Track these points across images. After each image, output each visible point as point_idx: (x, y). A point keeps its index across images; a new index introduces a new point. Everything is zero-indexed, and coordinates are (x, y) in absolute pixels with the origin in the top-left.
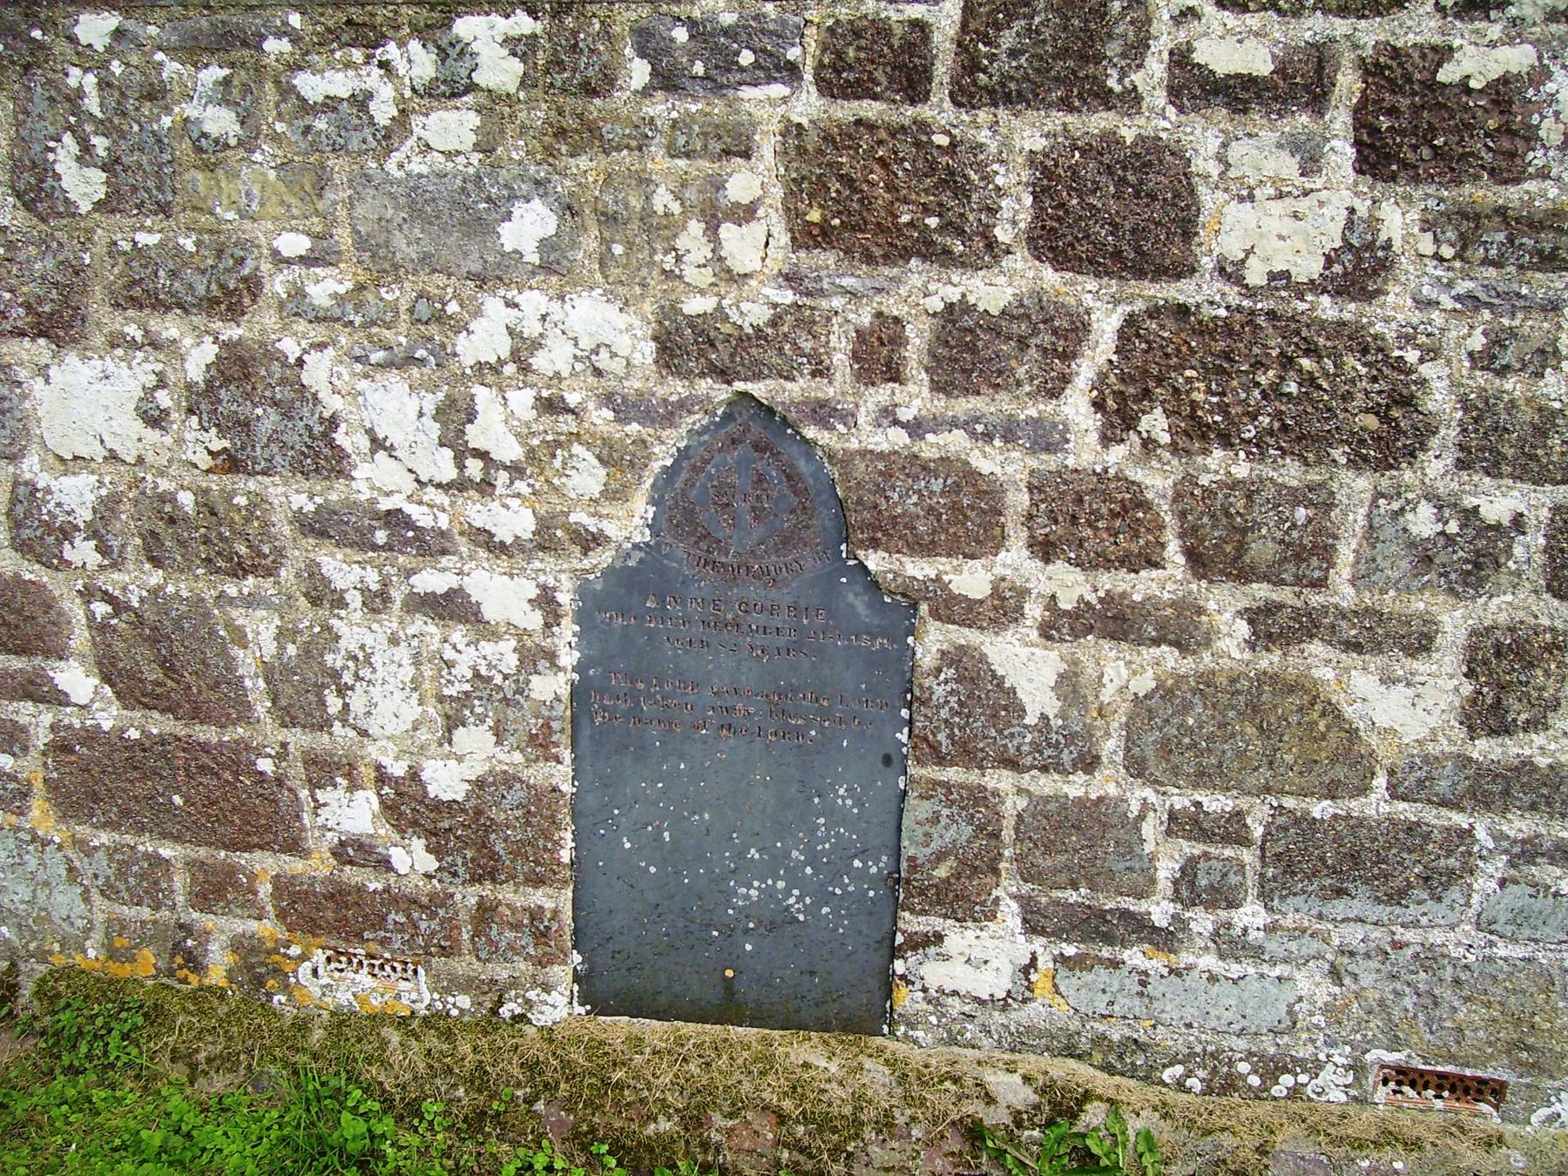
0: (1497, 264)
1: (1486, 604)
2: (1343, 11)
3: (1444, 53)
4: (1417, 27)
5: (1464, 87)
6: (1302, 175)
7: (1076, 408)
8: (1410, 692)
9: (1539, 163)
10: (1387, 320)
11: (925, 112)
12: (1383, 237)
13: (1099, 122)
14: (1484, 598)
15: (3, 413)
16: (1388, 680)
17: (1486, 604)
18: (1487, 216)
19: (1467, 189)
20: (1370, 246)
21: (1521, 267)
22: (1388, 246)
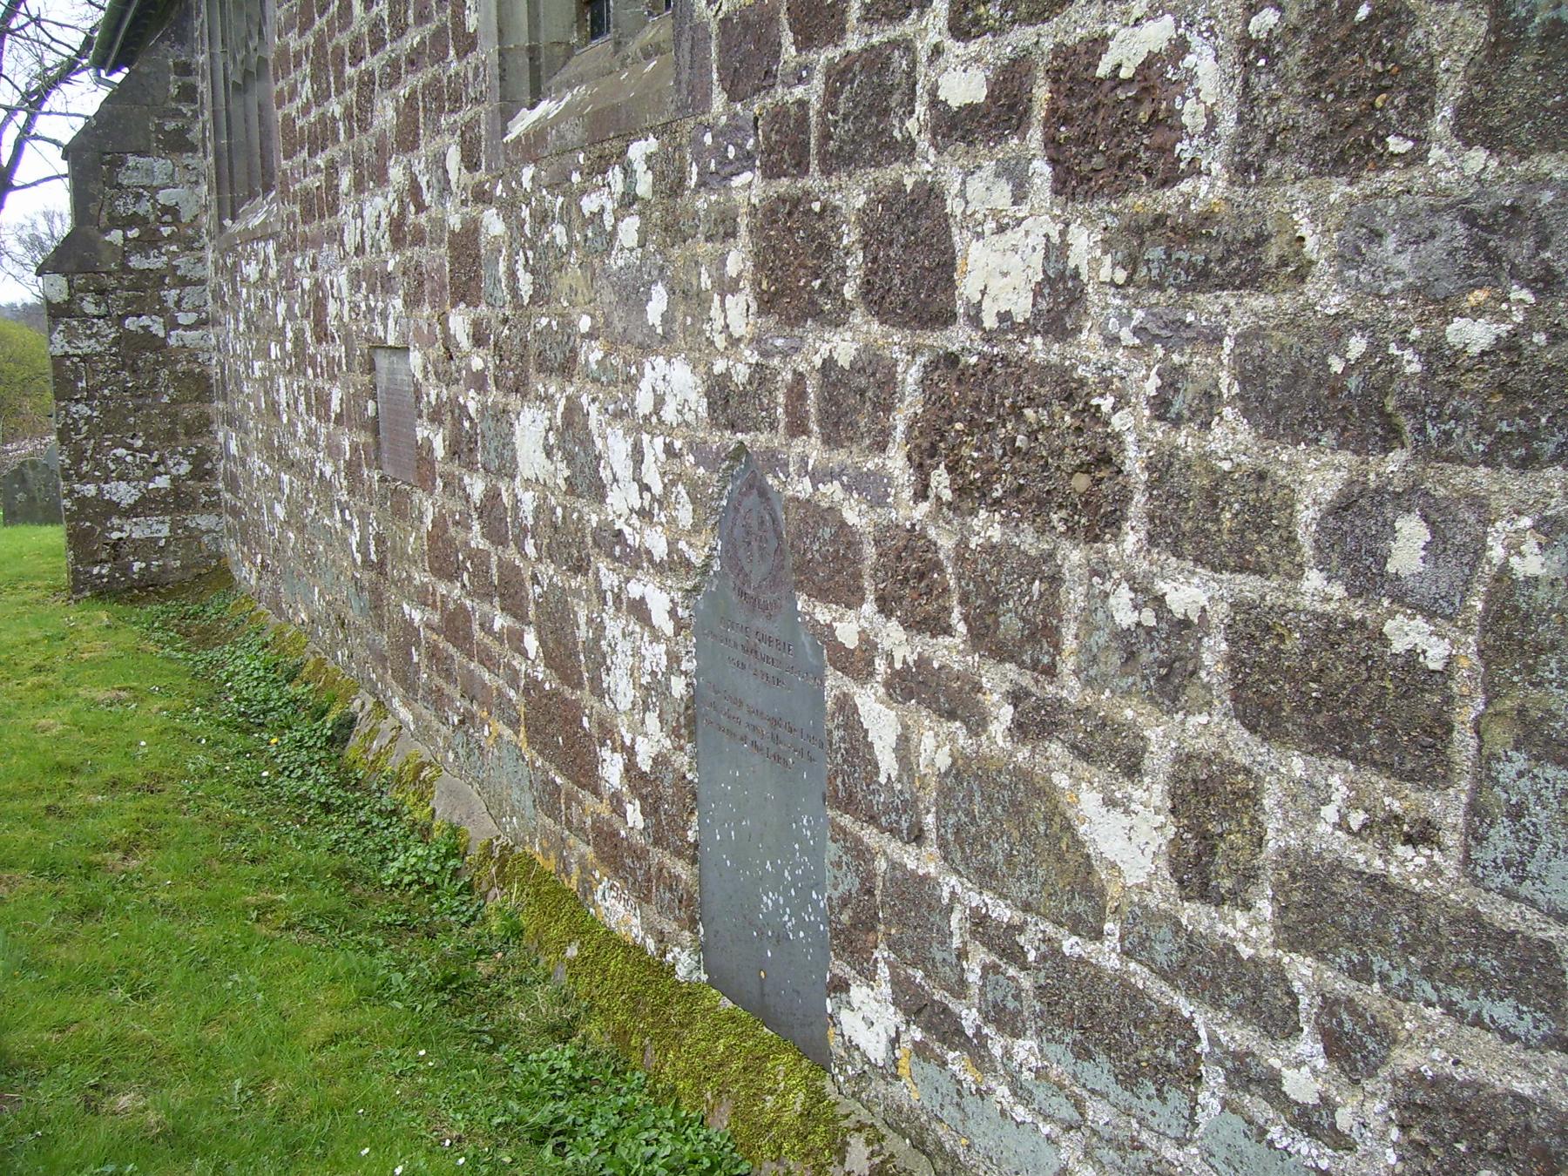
0: (1158, 286)
1: (1183, 723)
2: (1033, 18)
3: (1100, 43)
4: (1074, 25)
5: (1114, 79)
6: (1014, 203)
7: (896, 462)
8: (1126, 821)
9: (1187, 156)
10: (1087, 363)
11: (807, 182)
12: (1071, 264)
13: (893, 172)
14: (1180, 715)
15: (5, 1154)
16: (1110, 803)
17: (1183, 723)
18: (1150, 229)
19: (1131, 198)
20: (1062, 276)
21: (1179, 288)
22: (1076, 275)
